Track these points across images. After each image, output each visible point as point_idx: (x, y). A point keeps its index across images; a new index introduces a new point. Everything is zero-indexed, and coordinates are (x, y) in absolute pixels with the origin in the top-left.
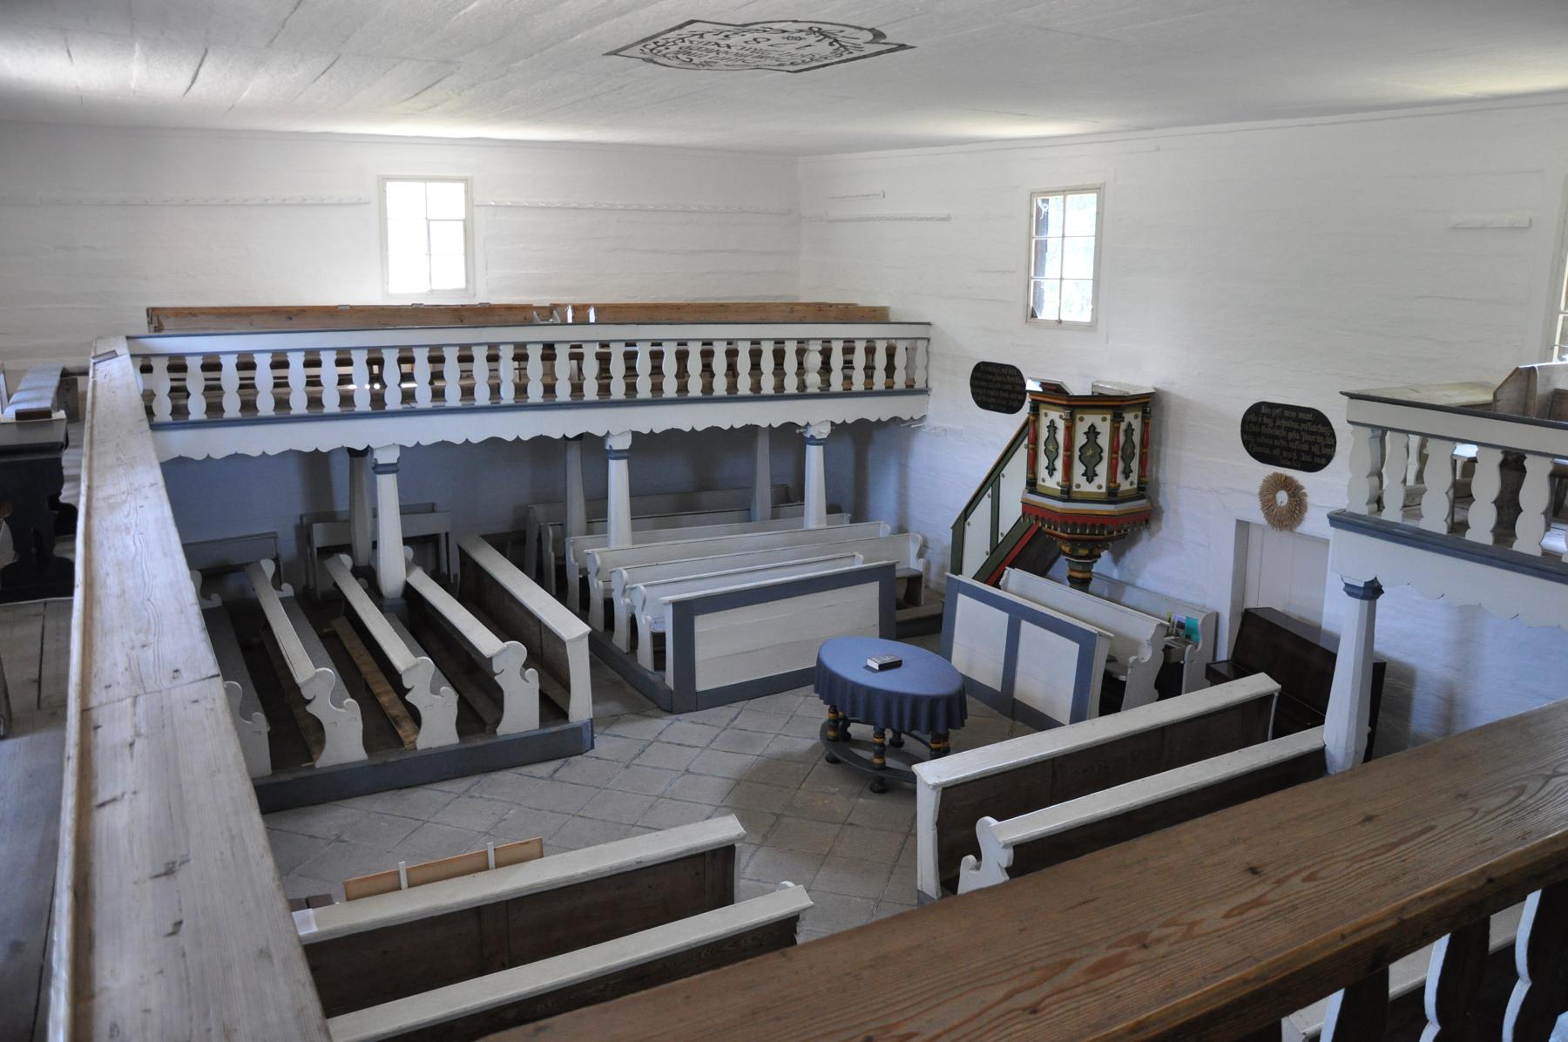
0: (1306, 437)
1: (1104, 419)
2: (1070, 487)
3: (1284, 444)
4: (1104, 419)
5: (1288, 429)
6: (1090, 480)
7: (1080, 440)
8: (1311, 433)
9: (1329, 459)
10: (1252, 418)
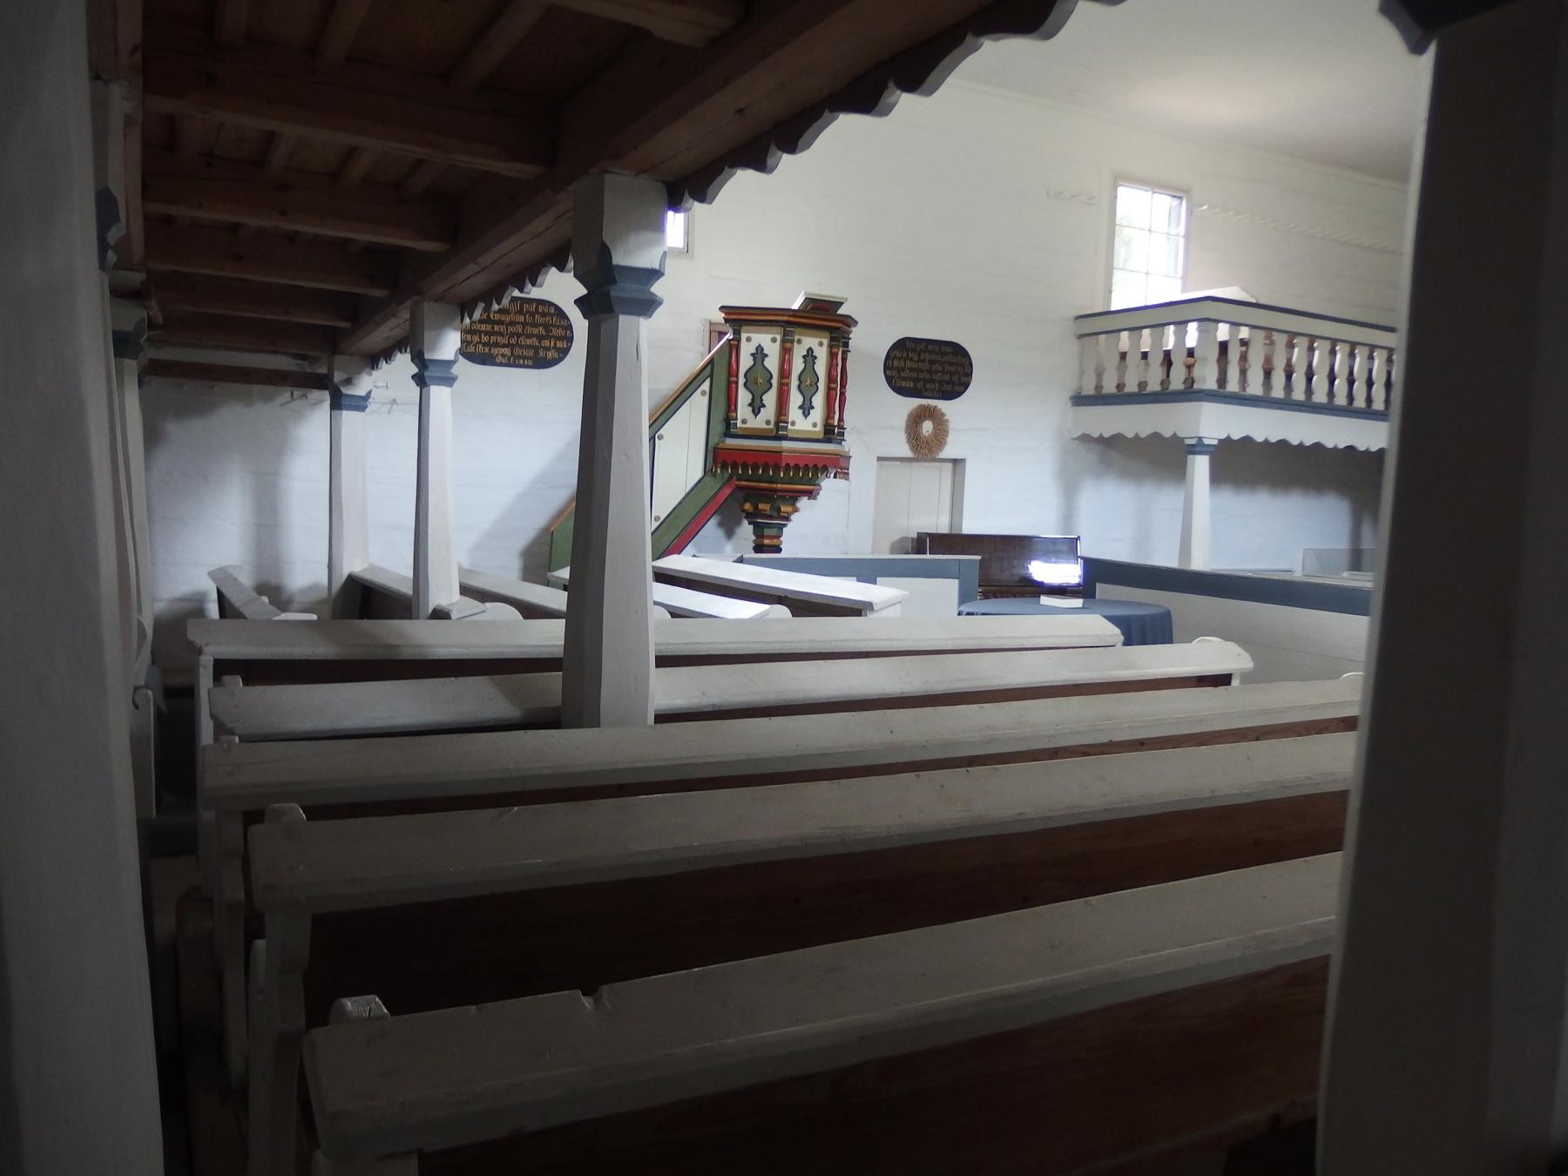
0: (947, 368)
1: (774, 340)
2: (783, 342)
3: (928, 376)
4: (744, 421)
5: (932, 362)
6: (760, 349)
7: (770, 399)
8: (951, 364)
9: (966, 386)
10: (897, 353)
